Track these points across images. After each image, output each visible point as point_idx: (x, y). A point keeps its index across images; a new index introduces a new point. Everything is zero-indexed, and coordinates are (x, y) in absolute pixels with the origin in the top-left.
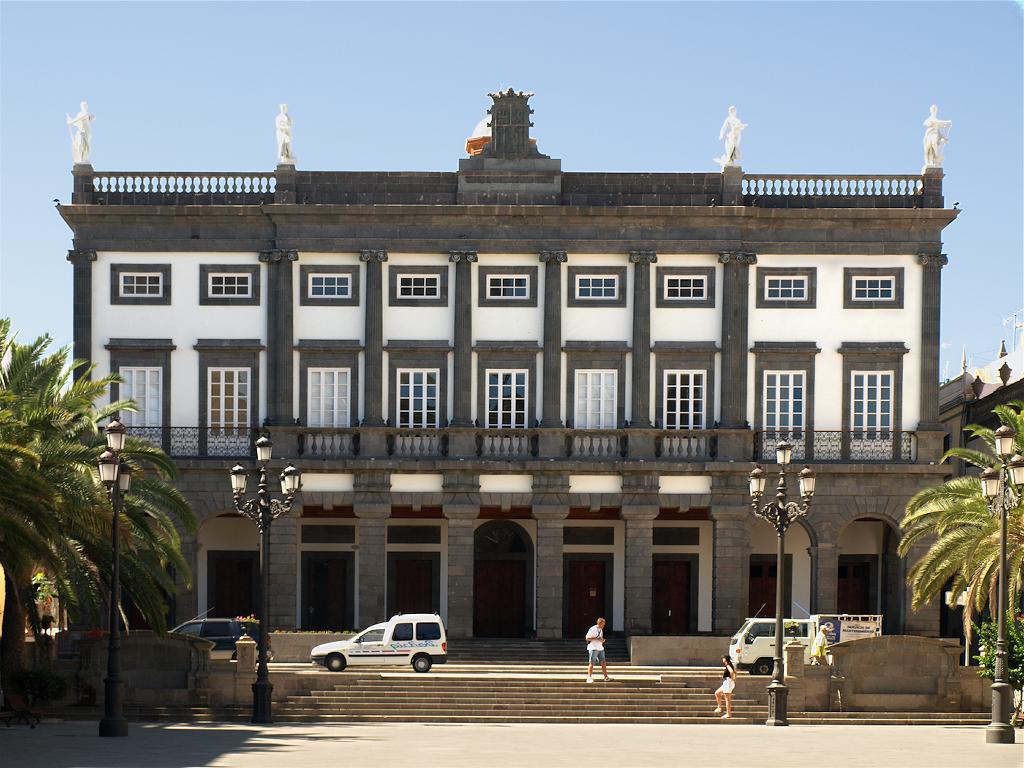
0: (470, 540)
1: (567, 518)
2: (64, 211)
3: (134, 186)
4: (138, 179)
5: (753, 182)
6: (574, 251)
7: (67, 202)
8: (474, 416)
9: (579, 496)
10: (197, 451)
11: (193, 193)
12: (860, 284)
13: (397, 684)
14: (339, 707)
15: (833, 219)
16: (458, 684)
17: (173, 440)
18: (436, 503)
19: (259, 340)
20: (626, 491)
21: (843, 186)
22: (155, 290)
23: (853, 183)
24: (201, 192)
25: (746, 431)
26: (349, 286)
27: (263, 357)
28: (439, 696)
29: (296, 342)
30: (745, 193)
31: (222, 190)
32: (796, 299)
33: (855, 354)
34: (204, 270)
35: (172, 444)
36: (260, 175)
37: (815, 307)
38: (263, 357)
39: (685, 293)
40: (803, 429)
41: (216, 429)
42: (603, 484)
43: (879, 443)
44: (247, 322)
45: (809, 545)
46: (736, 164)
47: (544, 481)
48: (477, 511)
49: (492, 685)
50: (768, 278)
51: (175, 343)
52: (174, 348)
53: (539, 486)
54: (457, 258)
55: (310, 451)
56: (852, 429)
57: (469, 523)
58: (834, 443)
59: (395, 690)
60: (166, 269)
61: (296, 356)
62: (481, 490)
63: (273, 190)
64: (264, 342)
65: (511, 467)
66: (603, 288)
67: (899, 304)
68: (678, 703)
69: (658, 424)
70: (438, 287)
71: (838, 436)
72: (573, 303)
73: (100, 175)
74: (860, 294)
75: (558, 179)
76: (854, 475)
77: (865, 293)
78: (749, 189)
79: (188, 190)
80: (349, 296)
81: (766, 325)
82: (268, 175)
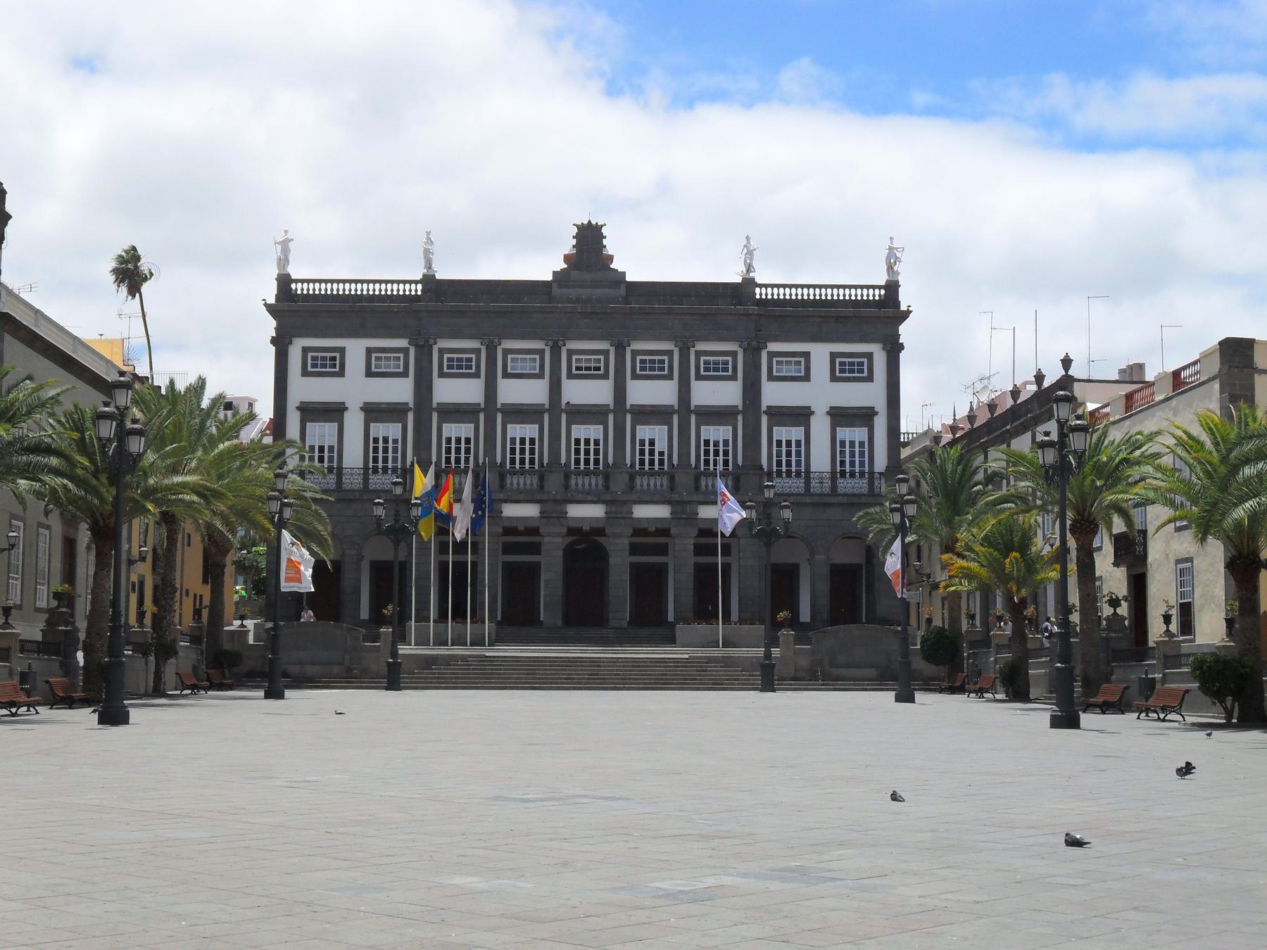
0: (560, 553)
1: (696, 537)
2: (269, 308)
3: (320, 290)
4: (359, 285)
5: (764, 289)
6: (635, 338)
7: (272, 300)
8: (563, 460)
9: (640, 520)
10: (361, 486)
11: (362, 294)
12: (450, 360)
13: (497, 661)
14: (452, 678)
15: (820, 317)
16: (541, 661)
17: (344, 477)
18: (535, 525)
19: (544, 404)
20: (674, 516)
21: (834, 293)
22: (333, 365)
23: (835, 291)
24: (368, 294)
25: (760, 472)
26: (474, 364)
27: (410, 416)
28: (526, 670)
29: (435, 405)
30: (758, 297)
31: (383, 293)
32: (651, 373)
33: (840, 416)
34: (833, 356)
35: (830, 482)
36: (410, 282)
37: (810, 381)
38: (410, 416)
39: (716, 372)
40: (803, 470)
41: (843, 474)
42: (529, 511)
43: (858, 481)
44: (400, 391)
45: (809, 558)
46: (751, 275)
47: (614, 509)
48: (565, 531)
49: (565, 662)
50: (310, 355)
51: (347, 405)
52: (813, 413)
53: (610, 513)
54: (551, 343)
55: (508, 485)
56: (371, 467)
57: (560, 540)
58: (348, 481)
59: (495, 665)
60: (342, 351)
61: (435, 416)
62: (503, 515)
63: (419, 293)
64: (411, 405)
65: (589, 498)
66: (657, 365)
67: (870, 378)
68: (700, 675)
69: (698, 466)
70: (338, 362)
71: (828, 476)
72: (635, 376)
73: (297, 281)
74: (642, 369)
75: (623, 286)
76: (840, 504)
77: (845, 371)
78: (761, 294)
79: (335, 292)
80: (473, 371)
81: (774, 394)
82: (416, 282)
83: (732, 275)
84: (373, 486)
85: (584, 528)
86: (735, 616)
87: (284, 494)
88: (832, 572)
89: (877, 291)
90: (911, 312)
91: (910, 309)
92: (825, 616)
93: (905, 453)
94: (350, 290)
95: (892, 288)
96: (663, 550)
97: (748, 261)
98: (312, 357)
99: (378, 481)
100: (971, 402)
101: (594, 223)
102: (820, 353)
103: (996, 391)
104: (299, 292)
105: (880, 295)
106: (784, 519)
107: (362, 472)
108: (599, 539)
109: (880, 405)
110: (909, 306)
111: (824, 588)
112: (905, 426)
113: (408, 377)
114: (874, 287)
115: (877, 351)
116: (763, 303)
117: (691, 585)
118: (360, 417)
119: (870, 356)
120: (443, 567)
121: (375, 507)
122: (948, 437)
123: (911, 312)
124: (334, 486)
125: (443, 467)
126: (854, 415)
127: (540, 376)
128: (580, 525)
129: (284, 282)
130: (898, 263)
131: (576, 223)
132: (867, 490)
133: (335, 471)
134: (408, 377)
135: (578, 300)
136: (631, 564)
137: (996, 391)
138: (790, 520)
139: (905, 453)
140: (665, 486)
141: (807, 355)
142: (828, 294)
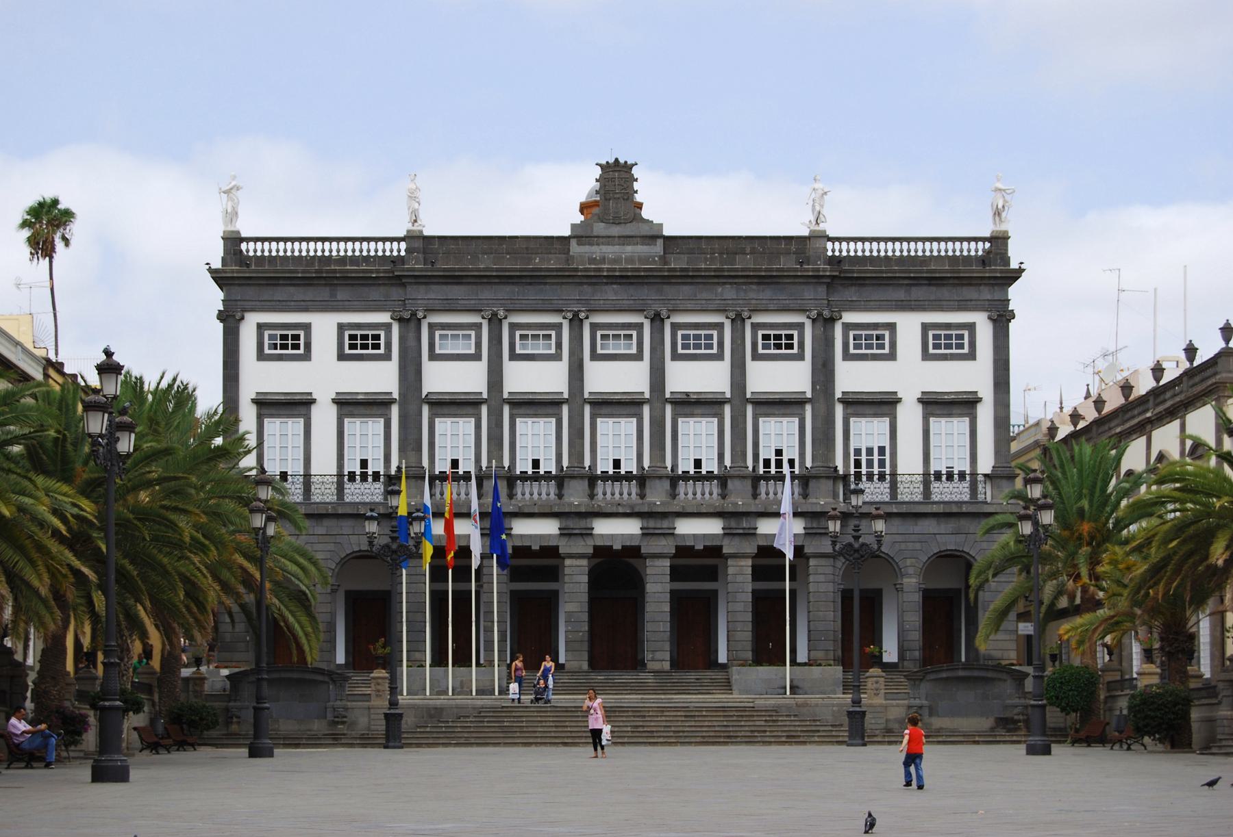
0: (585, 579)
7: (217, 264)
10: (335, 497)
18: (553, 543)
21: (873, 248)
27: (395, 411)
30: (830, 253)
33: (935, 405)
34: (925, 327)
36: (392, 240)
40: (888, 472)
48: (591, 551)
58: (318, 491)
60: (307, 327)
63: (403, 253)
67: (972, 356)
71: (920, 478)
72: (676, 357)
73: (248, 240)
78: (833, 251)
82: (399, 240)
83: (797, 227)
84: (350, 497)
85: (614, 548)
86: (802, 657)
87: (269, 505)
88: (924, 597)
89: (980, 244)
90: (1024, 270)
91: (1023, 266)
92: (917, 654)
93: (1015, 447)
94: (316, 251)
95: (999, 241)
96: (712, 574)
97: (818, 208)
98: (350, 335)
99: (876, 490)
100: (1088, 385)
101: (622, 161)
102: (909, 325)
103: (1122, 370)
104: (251, 254)
105: (984, 250)
106: (876, 532)
107: (335, 480)
108: (632, 561)
109: (986, 392)
110: (1022, 263)
111: (915, 619)
112: (1016, 419)
113: (561, 360)
114: (976, 240)
115: (982, 322)
116: (836, 261)
117: (749, 617)
118: (918, 410)
119: (971, 327)
120: (439, 599)
121: (367, 523)
122: (1064, 430)
123: (1024, 270)
124: (919, 496)
125: (761, 472)
126: (952, 403)
127: (477, 357)
128: (528, 544)
129: (233, 242)
130: (1006, 208)
131: (600, 162)
132: (968, 496)
133: (968, 478)
134: (561, 360)
135: (603, 260)
136: (512, 592)
137: (1122, 370)
138: (883, 534)
139: (1015, 447)
140: (715, 495)
141: (892, 327)
142: (918, 249)
